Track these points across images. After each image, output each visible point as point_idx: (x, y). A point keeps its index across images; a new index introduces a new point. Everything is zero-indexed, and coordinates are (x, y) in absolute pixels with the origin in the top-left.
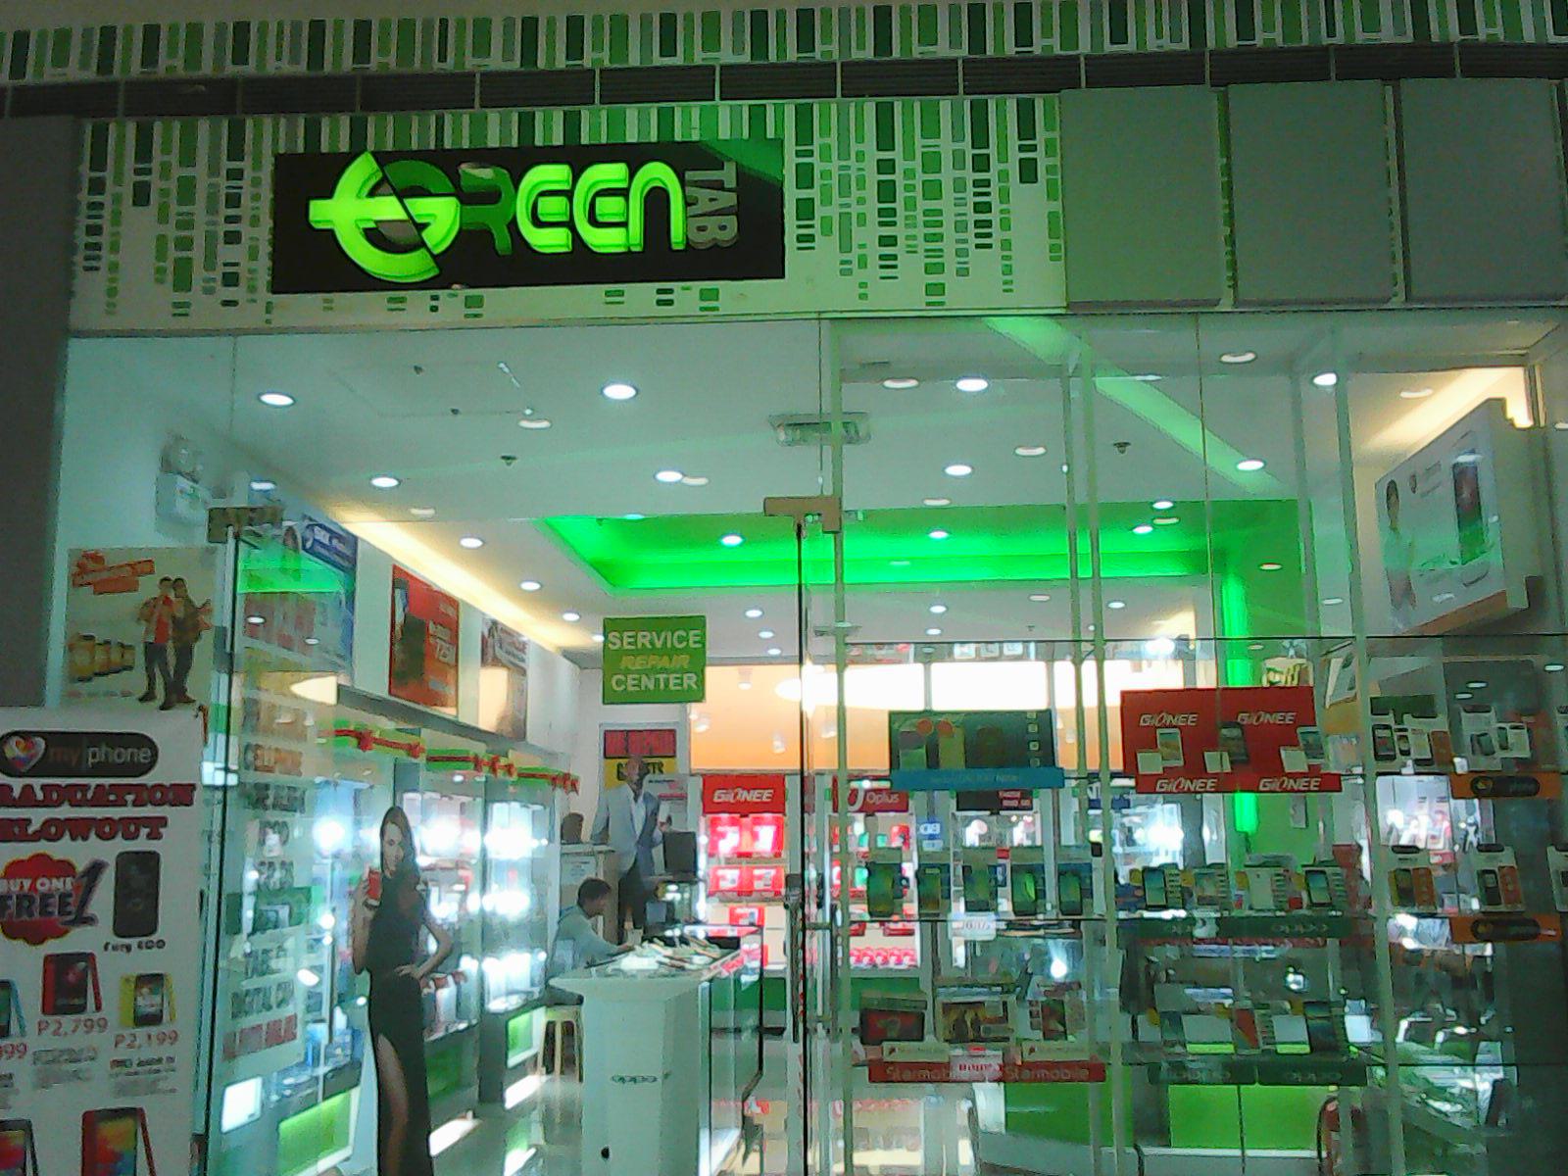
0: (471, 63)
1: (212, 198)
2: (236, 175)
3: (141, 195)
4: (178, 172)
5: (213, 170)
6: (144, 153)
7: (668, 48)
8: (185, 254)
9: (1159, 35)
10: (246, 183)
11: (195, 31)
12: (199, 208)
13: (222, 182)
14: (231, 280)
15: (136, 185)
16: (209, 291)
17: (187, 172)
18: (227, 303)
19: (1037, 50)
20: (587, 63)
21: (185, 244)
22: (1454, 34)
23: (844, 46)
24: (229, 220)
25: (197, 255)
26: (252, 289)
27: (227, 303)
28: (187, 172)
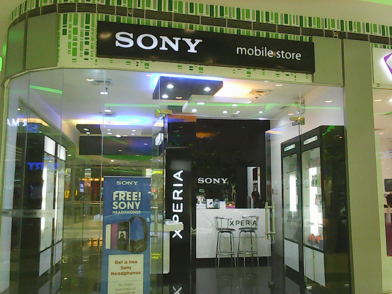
0: (198, 14)
1: (82, 33)
2: (87, 27)
3: (65, 32)
4: (73, 26)
5: (82, 27)
6: (65, 22)
7: (192, 11)
8: (75, 47)
9: (294, 23)
10: (90, 29)
11: (276, 14)
12: (79, 35)
13: (84, 29)
14: (87, 53)
15: (63, 30)
16: (81, 56)
17: (75, 26)
18: (85, 59)
19: (270, 22)
20: (224, 17)
21: (75, 44)
22: (116, 5)
23: (230, 15)
24: (86, 38)
25: (78, 47)
26: (92, 56)
27: (85, 59)
28: (75, 26)
